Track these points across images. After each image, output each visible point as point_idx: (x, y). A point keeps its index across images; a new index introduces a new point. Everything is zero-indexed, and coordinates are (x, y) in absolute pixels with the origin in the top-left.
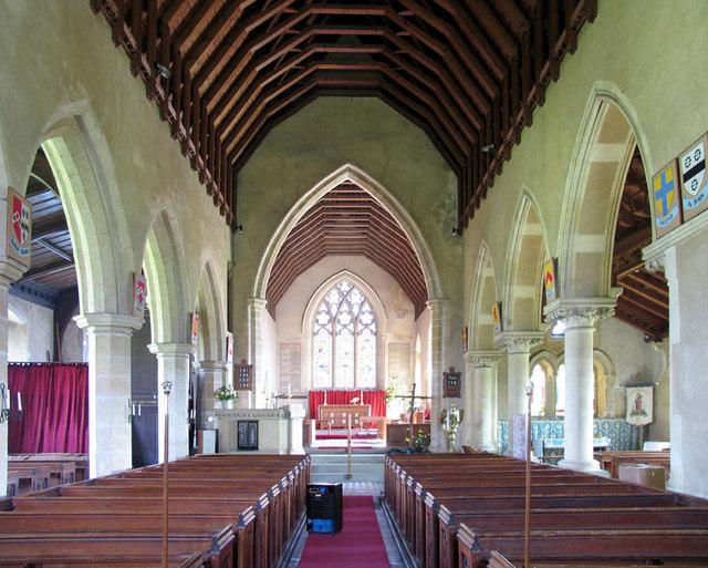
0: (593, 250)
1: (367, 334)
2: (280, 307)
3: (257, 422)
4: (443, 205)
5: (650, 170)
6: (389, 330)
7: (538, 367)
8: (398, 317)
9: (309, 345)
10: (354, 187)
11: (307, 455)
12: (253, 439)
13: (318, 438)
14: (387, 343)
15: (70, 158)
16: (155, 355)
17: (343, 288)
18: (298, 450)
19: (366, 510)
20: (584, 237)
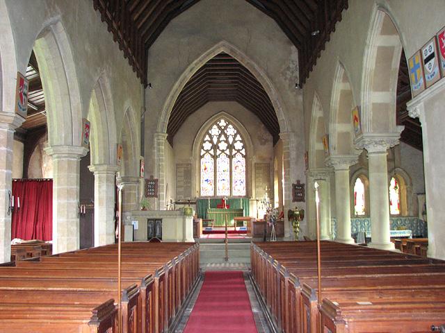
0: (382, 102)
1: (239, 157)
2: (178, 136)
3: (161, 220)
4: (288, 68)
5: (408, 56)
6: (255, 154)
7: (359, 180)
8: (261, 144)
9: (197, 166)
10: (227, 55)
11: (195, 243)
12: (157, 234)
13: (204, 233)
14: (253, 163)
15: (48, 50)
16: (93, 173)
17: (221, 124)
18: (190, 239)
19: (238, 280)
20: (376, 93)
